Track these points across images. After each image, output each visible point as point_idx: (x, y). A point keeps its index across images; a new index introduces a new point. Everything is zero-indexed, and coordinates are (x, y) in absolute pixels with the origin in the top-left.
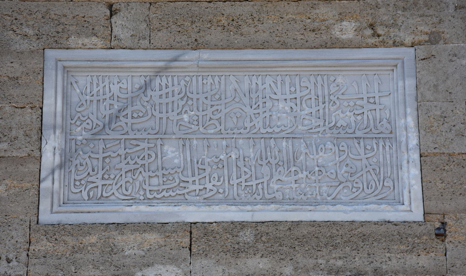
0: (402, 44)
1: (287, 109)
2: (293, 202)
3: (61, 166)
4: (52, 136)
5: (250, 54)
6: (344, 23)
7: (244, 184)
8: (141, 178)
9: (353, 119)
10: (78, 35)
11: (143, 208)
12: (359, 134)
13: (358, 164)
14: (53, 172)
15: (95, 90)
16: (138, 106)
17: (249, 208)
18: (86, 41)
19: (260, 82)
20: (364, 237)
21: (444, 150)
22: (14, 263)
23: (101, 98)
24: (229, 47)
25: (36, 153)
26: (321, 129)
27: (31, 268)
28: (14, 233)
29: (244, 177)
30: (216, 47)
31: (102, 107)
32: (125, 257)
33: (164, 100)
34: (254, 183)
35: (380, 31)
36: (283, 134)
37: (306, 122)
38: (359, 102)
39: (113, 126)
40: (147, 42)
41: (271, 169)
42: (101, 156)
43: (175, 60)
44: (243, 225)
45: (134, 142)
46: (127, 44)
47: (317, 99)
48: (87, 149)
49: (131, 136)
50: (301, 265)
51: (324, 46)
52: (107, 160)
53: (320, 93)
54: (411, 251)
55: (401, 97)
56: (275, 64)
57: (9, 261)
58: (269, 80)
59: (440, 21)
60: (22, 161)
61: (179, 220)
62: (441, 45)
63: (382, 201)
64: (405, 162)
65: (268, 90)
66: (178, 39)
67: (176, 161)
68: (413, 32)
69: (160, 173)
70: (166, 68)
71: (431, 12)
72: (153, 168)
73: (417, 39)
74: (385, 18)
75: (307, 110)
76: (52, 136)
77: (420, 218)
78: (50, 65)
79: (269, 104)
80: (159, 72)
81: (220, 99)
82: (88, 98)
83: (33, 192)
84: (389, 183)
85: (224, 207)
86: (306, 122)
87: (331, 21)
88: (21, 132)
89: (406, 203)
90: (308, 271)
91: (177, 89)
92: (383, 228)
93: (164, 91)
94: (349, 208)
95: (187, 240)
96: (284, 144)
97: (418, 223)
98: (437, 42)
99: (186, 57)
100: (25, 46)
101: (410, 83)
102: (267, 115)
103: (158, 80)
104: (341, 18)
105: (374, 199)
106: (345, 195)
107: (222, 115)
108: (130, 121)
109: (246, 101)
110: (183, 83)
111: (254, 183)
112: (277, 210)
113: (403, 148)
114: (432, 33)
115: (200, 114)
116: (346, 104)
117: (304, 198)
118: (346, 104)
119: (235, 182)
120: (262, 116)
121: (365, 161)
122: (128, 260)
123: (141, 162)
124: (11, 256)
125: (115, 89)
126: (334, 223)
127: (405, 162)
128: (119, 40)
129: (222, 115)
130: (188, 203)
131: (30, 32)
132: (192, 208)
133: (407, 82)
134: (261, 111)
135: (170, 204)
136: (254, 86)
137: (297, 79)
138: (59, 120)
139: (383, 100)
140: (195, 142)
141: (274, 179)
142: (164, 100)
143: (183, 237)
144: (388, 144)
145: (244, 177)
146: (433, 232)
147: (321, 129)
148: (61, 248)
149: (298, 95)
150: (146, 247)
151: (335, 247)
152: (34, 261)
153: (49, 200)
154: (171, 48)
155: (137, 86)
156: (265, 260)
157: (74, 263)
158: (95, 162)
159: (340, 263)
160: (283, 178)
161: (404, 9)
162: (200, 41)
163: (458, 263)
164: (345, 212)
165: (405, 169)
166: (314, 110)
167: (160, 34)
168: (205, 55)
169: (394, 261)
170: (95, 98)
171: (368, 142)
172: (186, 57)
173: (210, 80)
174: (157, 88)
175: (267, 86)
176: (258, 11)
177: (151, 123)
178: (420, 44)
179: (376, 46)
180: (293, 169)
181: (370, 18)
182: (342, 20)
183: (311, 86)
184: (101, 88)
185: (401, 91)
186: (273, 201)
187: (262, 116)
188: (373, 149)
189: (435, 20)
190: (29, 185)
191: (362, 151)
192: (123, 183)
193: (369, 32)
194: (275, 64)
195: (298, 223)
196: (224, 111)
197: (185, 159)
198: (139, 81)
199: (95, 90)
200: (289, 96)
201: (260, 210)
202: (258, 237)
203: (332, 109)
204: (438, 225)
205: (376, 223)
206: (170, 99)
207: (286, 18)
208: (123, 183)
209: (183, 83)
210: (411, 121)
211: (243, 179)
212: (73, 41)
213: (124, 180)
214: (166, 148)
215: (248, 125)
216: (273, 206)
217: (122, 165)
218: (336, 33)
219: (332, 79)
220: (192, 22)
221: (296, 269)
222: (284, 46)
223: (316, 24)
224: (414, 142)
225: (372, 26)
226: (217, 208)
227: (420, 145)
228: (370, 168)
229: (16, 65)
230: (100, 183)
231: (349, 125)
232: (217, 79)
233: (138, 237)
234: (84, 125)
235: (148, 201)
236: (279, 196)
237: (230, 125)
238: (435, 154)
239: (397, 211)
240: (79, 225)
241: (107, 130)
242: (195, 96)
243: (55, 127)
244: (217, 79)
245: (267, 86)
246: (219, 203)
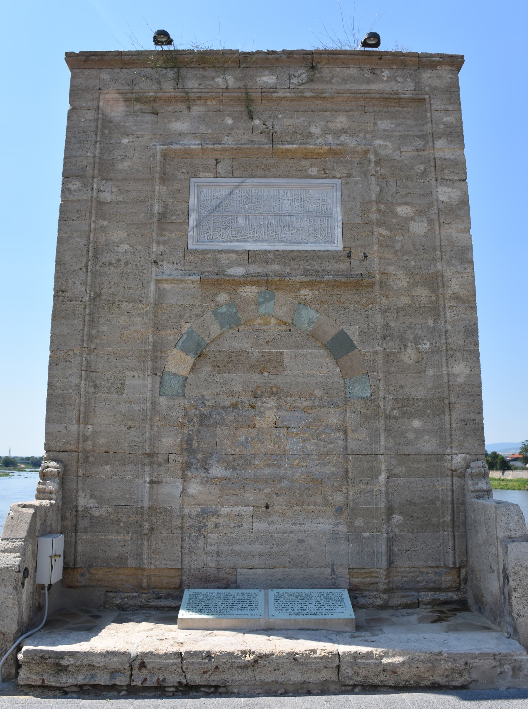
0: (336, 178)
1: (289, 203)
2: (290, 242)
3: (196, 226)
4: (193, 214)
5: (274, 180)
6: (313, 168)
7: (270, 234)
8: (228, 231)
9: (315, 208)
10: (204, 172)
11: (229, 244)
12: (318, 214)
13: (317, 227)
14: (193, 229)
15: (210, 195)
16: (227, 202)
17: (272, 244)
18: (207, 174)
19: (277, 192)
20: (319, 257)
21: (351, 222)
22: (179, 265)
23: (213, 198)
24: (265, 177)
25: (187, 221)
26: (302, 212)
27: (185, 267)
28: (178, 253)
29: (270, 232)
30: (260, 177)
31: (213, 202)
32: (222, 263)
33: (238, 199)
34: (274, 234)
35: (327, 172)
36: (287, 214)
37: (296, 209)
38: (318, 201)
39: (217, 210)
40: (231, 175)
41: (282, 228)
42: (212, 222)
43: (243, 182)
44: (270, 251)
45: (226, 217)
46: (223, 176)
47: (301, 200)
48: (206, 219)
49: (225, 214)
50: (293, 268)
51: (305, 177)
52: (215, 224)
53: (302, 197)
54: (337, 263)
55: (335, 200)
56: (284, 184)
57: (177, 264)
58: (281, 191)
59: (351, 169)
60: (181, 224)
61: (244, 249)
62: (351, 179)
63: (326, 242)
64: (336, 226)
65: (281, 195)
66: (244, 173)
67: (243, 224)
68: (340, 173)
69: (236, 229)
70: (239, 186)
71: (348, 165)
72: (233, 227)
73: (342, 175)
74: (329, 166)
75: (297, 204)
76: (193, 214)
77: (341, 249)
78: (192, 184)
79: (281, 201)
80: (236, 187)
81: (261, 199)
82: (207, 198)
83: (186, 236)
84: (329, 235)
85: (262, 244)
86: (296, 209)
87: (307, 167)
88: (181, 212)
89: (336, 243)
90: (296, 270)
91: (243, 194)
92: (326, 253)
93: (238, 195)
94: (313, 245)
95: (247, 257)
96: (287, 218)
97: (341, 251)
98: (350, 177)
99: (247, 181)
100: (182, 176)
101: (339, 194)
102: (280, 205)
103: (235, 191)
104: (312, 166)
105: (323, 241)
106: (312, 239)
107: (262, 206)
108: (224, 207)
109: (272, 200)
110: (246, 192)
111: (274, 234)
112: (284, 245)
113: (336, 221)
114: (348, 173)
115: (253, 205)
116: (313, 202)
117: (295, 241)
118: (313, 202)
119: (267, 233)
120: (278, 206)
121: (320, 226)
122: (223, 265)
123: (228, 225)
124: (178, 262)
125: (218, 194)
126: (307, 251)
127: (336, 226)
128: (220, 174)
129: (262, 206)
130: (248, 242)
131: (185, 171)
132: (248, 244)
133: (338, 193)
134: (278, 204)
135: (240, 242)
136: (275, 194)
137: (293, 191)
138: (196, 207)
139: (328, 200)
140: (250, 217)
141: (283, 232)
142: (238, 199)
143: (245, 256)
144: (329, 219)
145: (270, 232)
146: (346, 255)
147: (302, 212)
148: (197, 259)
149: (293, 197)
150: (231, 260)
151: (307, 261)
152: (187, 264)
153: (192, 240)
154: (241, 177)
155: (227, 193)
156: (278, 266)
157: (202, 265)
158: (210, 224)
159: (309, 267)
160: (287, 232)
161: (337, 163)
162: (253, 174)
163: (355, 267)
164: (311, 246)
165: (336, 229)
166: (300, 204)
167: (237, 171)
168: (255, 180)
169: (330, 266)
170: (210, 198)
171: (321, 218)
172: (247, 181)
173: (257, 191)
174: (235, 194)
175: (280, 193)
176: (277, 162)
177: (232, 209)
178: (343, 177)
179: (326, 178)
180: (291, 228)
181: (323, 166)
182: (312, 167)
183: (299, 194)
184: (212, 194)
185: (335, 197)
186: (282, 242)
187: (278, 206)
188: (323, 221)
189: (349, 168)
190: (184, 234)
191: (319, 221)
192: (221, 233)
193: (323, 172)
194: (284, 184)
195: (292, 251)
196: (263, 204)
197: (246, 224)
198: (228, 191)
199: (210, 195)
200: (289, 198)
201: (277, 245)
202: (276, 256)
203: (307, 204)
204: (348, 252)
205: (324, 251)
206: (240, 199)
207: (289, 165)
208: (221, 233)
209: (246, 192)
210: (339, 210)
211: (270, 232)
212: (201, 174)
213: (222, 232)
214: (238, 219)
215: (272, 210)
216: (282, 244)
217: (221, 226)
218: (309, 172)
219: (307, 191)
220: (250, 167)
221: (291, 269)
222: (288, 177)
223: (301, 168)
224: (340, 218)
225: (324, 170)
226: (259, 244)
227: (342, 219)
228: (322, 229)
229: (179, 185)
230: (212, 233)
231: (314, 211)
232: (260, 191)
233: (227, 255)
234: (206, 209)
235: (231, 241)
236: (285, 239)
237: (265, 210)
238: (348, 223)
239: (332, 246)
240: (204, 250)
241: (215, 212)
242: (250, 198)
243: (194, 210)
244: (260, 191)
245: (280, 193)
246: (261, 242)
